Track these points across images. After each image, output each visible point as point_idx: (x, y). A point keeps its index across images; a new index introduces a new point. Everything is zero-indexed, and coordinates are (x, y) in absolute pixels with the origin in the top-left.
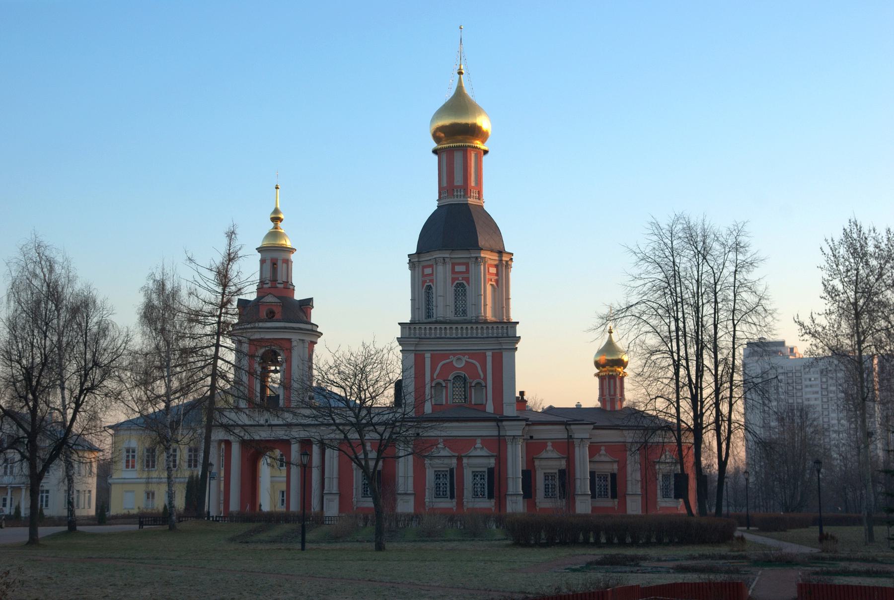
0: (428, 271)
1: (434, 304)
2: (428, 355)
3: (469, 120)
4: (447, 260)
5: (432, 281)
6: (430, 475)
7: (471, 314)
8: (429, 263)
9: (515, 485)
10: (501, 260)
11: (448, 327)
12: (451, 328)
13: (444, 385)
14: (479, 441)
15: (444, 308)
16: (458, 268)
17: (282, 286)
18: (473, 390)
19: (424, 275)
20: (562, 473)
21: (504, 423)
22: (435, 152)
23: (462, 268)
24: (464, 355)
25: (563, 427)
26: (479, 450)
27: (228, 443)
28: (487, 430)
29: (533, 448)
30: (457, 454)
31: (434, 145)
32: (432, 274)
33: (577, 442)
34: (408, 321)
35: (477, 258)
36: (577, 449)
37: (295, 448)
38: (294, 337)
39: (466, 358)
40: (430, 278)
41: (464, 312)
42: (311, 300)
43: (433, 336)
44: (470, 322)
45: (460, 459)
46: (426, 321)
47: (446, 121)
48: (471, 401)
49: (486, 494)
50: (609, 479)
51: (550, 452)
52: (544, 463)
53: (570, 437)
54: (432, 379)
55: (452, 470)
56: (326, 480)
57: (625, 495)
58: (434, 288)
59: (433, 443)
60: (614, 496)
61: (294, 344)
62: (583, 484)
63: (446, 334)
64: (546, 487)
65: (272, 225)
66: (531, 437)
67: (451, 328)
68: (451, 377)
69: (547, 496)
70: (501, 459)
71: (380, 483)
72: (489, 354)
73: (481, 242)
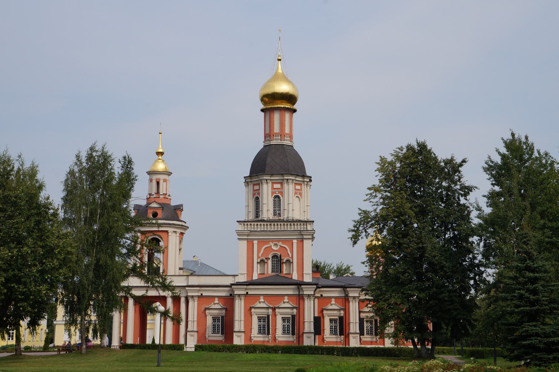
0: (256, 187)
2: (255, 242)
4: (268, 181)
5: (259, 194)
6: (209, 321)
7: (284, 216)
8: (257, 182)
9: (309, 327)
12: (257, 225)
13: (266, 261)
14: (333, 300)
15: (267, 212)
16: (276, 186)
17: (163, 196)
18: (284, 265)
19: (254, 190)
20: (341, 318)
21: (302, 286)
22: (262, 110)
23: (278, 186)
24: (279, 241)
25: (342, 289)
28: (290, 291)
30: (271, 306)
31: (262, 106)
33: (351, 299)
38: (170, 230)
39: (280, 244)
41: (279, 214)
42: (182, 205)
43: (259, 229)
45: (274, 309)
46: (255, 220)
49: (374, 334)
54: (258, 257)
55: (268, 316)
56: (189, 323)
57: (349, 334)
58: (260, 200)
60: (341, 334)
61: (170, 234)
62: (354, 327)
63: (281, 228)
67: (257, 225)
68: (270, 257)
69: (331, 333)
70: (346, 309)
71: (225, 325)
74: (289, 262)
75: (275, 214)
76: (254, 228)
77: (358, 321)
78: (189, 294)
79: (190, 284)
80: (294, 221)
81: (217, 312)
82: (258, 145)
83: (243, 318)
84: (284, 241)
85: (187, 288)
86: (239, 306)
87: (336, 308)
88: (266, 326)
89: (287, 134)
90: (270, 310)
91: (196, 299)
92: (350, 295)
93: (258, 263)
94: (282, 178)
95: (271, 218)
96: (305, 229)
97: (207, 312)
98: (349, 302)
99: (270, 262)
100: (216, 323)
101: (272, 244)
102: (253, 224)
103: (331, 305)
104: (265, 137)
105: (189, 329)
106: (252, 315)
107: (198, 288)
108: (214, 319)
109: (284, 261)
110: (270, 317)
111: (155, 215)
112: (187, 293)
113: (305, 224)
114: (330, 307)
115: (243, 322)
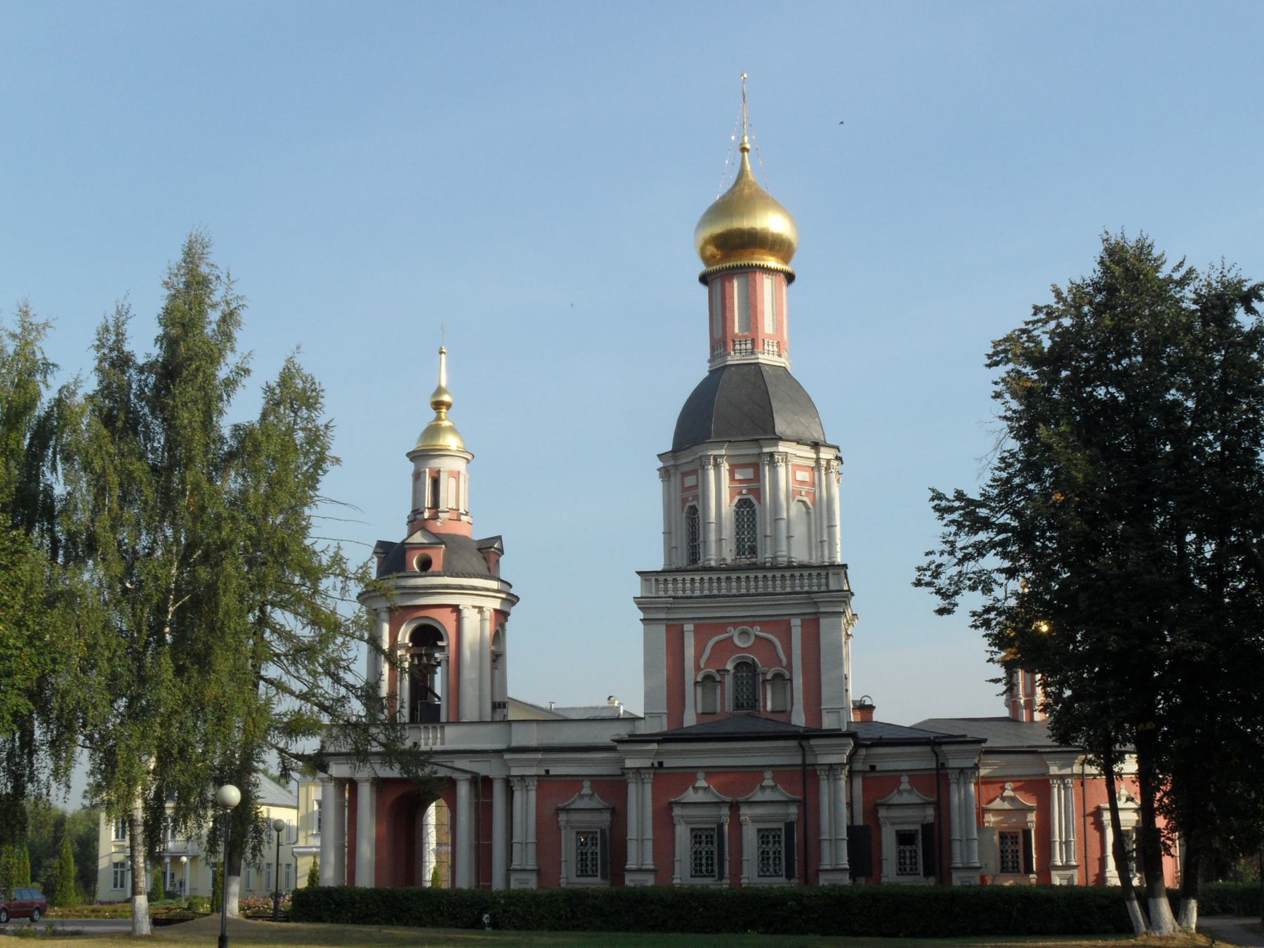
0: (690, 481)
1: (701, 539)
2: (689, 627)
3: (746, 224)
5: (696, 498)
6: (682, 834)
7: (765, 555)
8: (691, 467)
10: (818, 460)
11: (723, 576)
12: (728, 578)
13: (718, 678)
14: (768, 775)
15: (720, 545)
18: (769, 688)
19: (684, 489)
20: (927, 828)
21: (812, 742)
24: (752, 624)
25: (928, 749)
26: (587, 799)
27: (353, 784)
29: (877, 785)
30: (728, 799)
32: (696, 486)
33: (953, 776)
34: (659, 565)
35: (772, 455)
36: (954, 788)
37: (463, 790)
39: (757, 630)
40: (693, 492)
41: (753, 550)
42: (499, 538)
43: (697, 593)
44: (763, 567)
45: (735, 807)
47: (718, 229)
48: (765, 706)
49: (921, 868)
50: (1021, 840)
51: (906, 794)
52: (894, 813)
53: (941, 767)
54: (697, 668)
55: (721, 826)
56: (516, 848)
58: (700, 513)
59: (687, 776)
64: (764, 857)
65: (433, 414)
66: (873, 768)
68: (730, 666)
70: (618, 814)
72: (796, 622)
73: (780, 427)
74: (782, 680)
75: (740, 550)
76: (684, 591)
77: (844, 835)
78: (515, 771)
79: (514, 744)
80: (794, 567)
81: (588, 817)
82: (699, 371)
83: (649, 834)
84: (766, 623)
85: (507, 756)
86: (640, 804)
87: (914, 799)
88: (715, 853)
89: (770, 337)
90: (725, 811)
91: (533, 785)
92: (952, 763)
93: (696, 683)
94: (756, 451)
95: (729, 561)
96: (823, 588)
97: (563, 817)
98: (948, 785)
99: (729, 680)
100: (589, 849)
101: (733, 633)
102: (680, 578)
103: (900, 792)
104: (713, 349)
105: (516, 864)
106: (674, 825)
107: (540, 756)
108: (764, 835)
109: (769, 677)
110: (726, 827)
111: (425, 565)
112: (509, 768)
113: (823, 573)
114: (896, 799)
115: (649, 846)
